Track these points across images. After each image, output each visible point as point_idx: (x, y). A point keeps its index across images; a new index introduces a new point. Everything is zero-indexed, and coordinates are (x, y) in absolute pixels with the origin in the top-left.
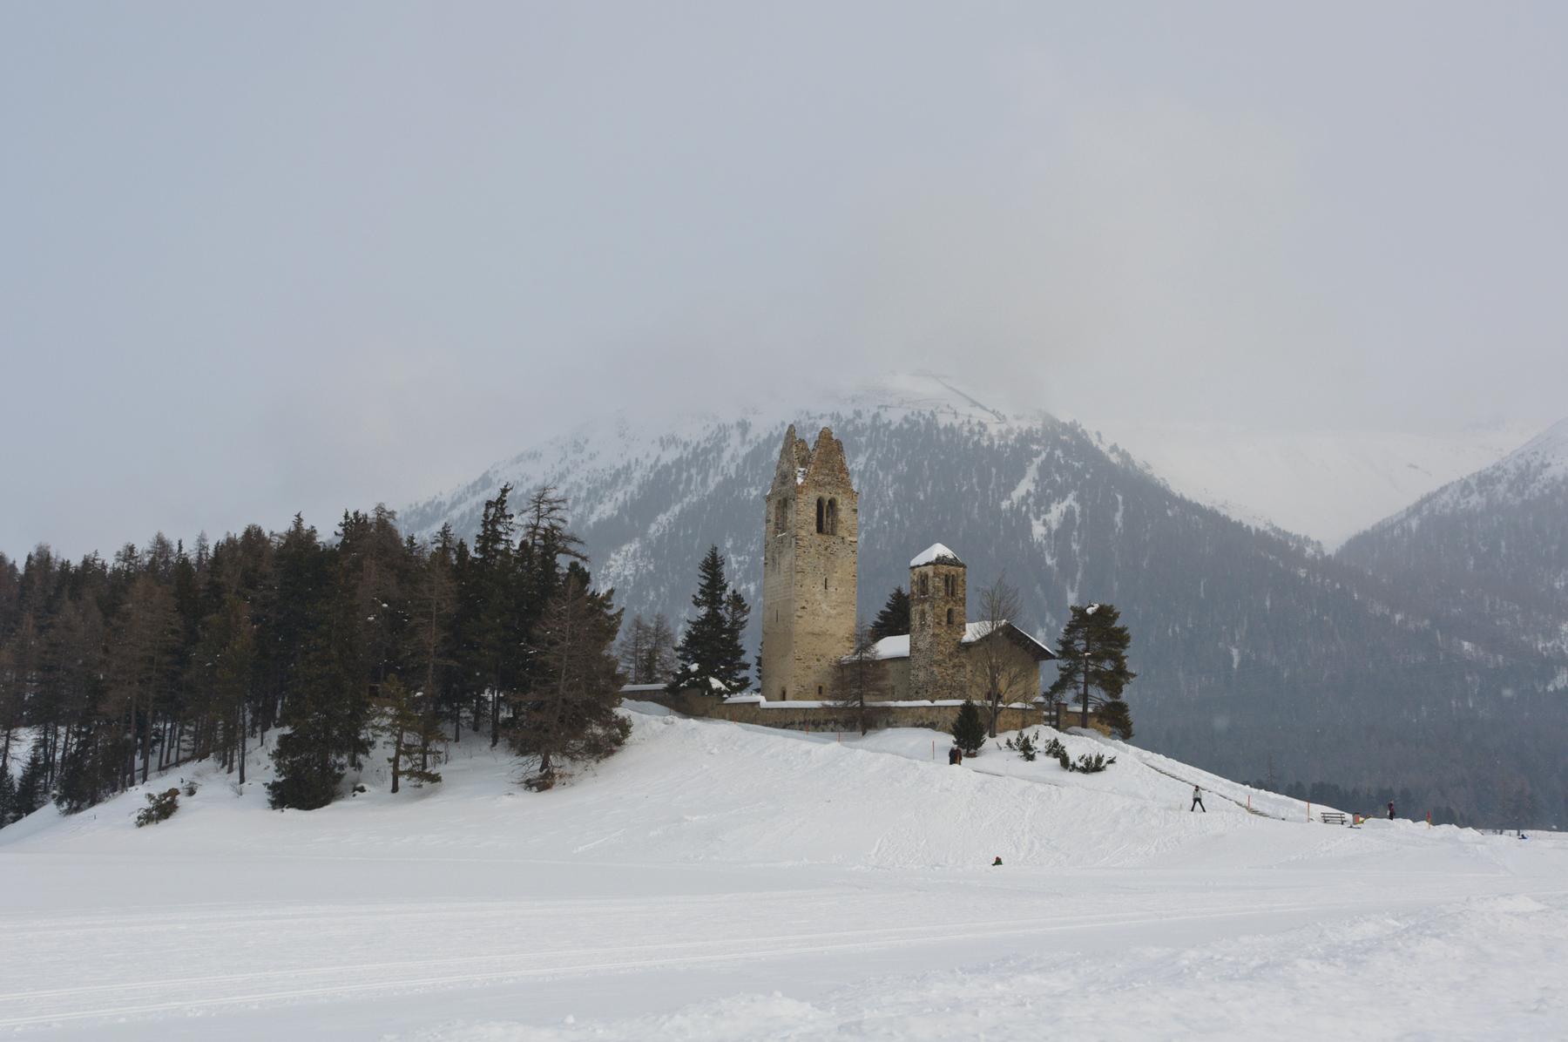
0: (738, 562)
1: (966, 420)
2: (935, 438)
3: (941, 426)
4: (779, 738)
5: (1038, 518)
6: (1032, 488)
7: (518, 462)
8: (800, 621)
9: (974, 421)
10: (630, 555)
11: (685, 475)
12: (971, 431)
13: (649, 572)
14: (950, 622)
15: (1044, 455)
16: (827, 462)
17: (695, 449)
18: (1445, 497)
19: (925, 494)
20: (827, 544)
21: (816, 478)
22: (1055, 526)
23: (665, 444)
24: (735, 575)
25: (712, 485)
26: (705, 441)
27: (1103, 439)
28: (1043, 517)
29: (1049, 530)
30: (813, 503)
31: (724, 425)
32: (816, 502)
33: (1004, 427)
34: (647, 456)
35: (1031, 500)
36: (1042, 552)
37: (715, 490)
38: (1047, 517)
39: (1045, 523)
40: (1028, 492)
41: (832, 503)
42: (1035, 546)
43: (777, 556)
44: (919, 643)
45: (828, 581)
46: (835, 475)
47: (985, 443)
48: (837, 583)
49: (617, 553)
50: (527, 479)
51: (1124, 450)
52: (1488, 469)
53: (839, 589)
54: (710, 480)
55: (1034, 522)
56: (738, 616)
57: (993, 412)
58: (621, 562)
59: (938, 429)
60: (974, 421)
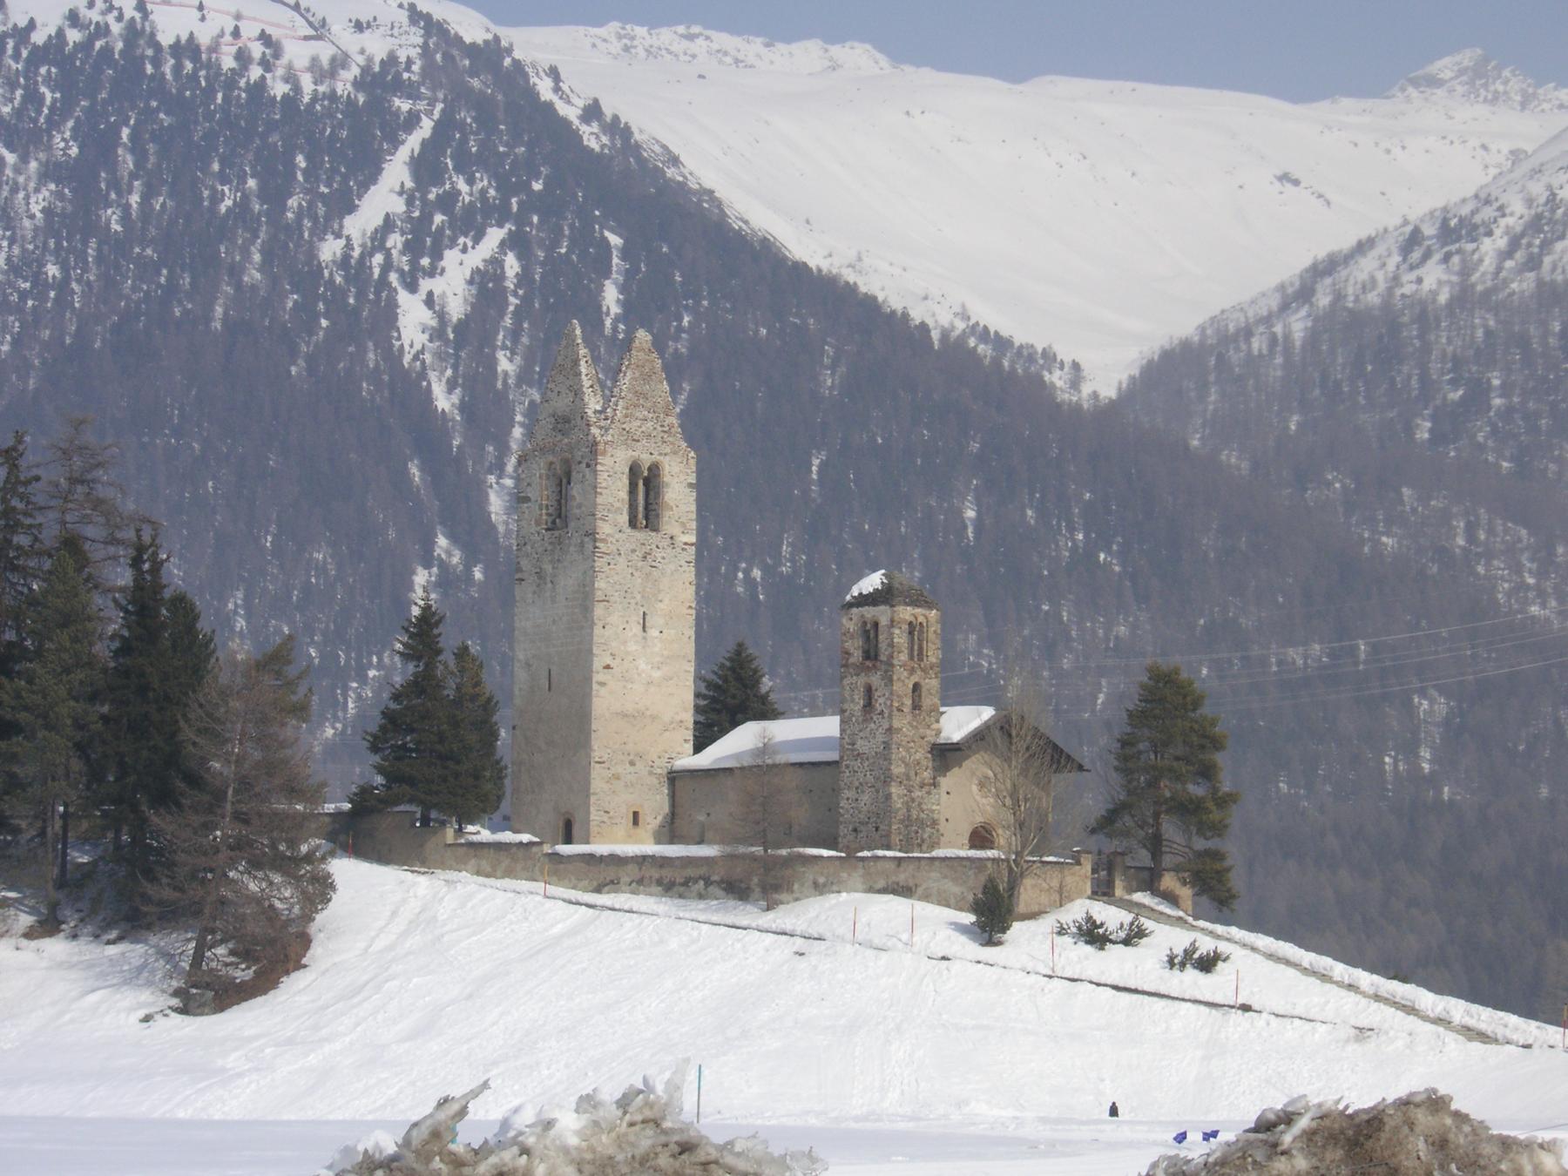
1: (229, 29)
3: (166, 39)
4: (501, 898)
5: (412, 287)
6: (398, 206)
8: (603, 691)
9: (250, 30)
12: (242, 57)
14: (916, 706)
15: (426, 127)
18: (1366, 266)
19: (126, 218)
22: (456, 309)
28: (425, 285)
29: (442, 316)
32: (627, 470)
33: (325, 52)
35: (395, 241)
36: (423, 375)
39: (430, 301)
41: (655, 469)
42: (407, 359)
43: (548, 568)
44: (859, 742)
45: (648, 618)
47: (279, 89)
51: (616, 118)
52: (1464, 201)
55: (403, 296)
57: (296, 7)
59: (157, 47)
60: (250, 30)
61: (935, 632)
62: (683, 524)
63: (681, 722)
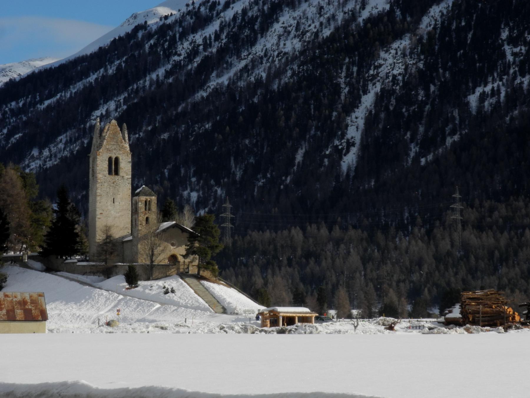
0: (514, 54)
10: (399, 53)
13: (419, 71)
16: (113, 138)
20: (114, 181)
21: (107, 147)
24: (509, 68)
30: (106, 160)
32: (107, 159)
41: (117, 159)
45: (115, 199)
46: (118, 144)
49: (386, 51)
53: (121, 203)
56: (75, 217)
58: (390, 61)
61: (155, 203)
62: (127, 173)
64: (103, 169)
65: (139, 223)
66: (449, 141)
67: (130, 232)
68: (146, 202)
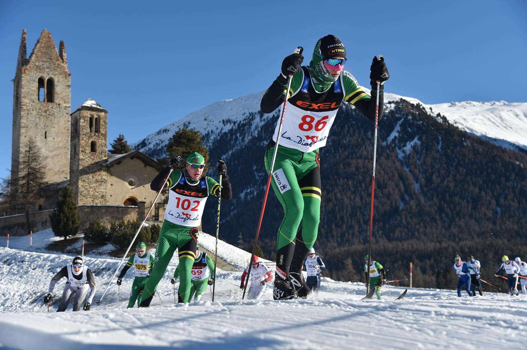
0: (259, 176)
2: (350, 113)
7: (158, 134)
11: (234, 137)
15: (403, 119)
17: (239, 125)
20: (46, 109)
21: (37, 64)
23: (225, 123)
25: (247, 140)
26: (243, 121)
27: (433, 111)
31: (252, 113)
32: (37, 80)
34: (217, 129)
37: (248, 143)
38: (405, 148)
39: (403, 151)
40: (395, 137)
41: (51, 82)
45: (47, 134)
46: (53, 62)
48: (54, 134)
50: (162, 142)
51: (443, 116)
54: (246, 139)
63: (63, 171)
64: (31, 92)
65: (81, 149)
66: (232, 214)
67: (69, 179)
68: (91, 119)
